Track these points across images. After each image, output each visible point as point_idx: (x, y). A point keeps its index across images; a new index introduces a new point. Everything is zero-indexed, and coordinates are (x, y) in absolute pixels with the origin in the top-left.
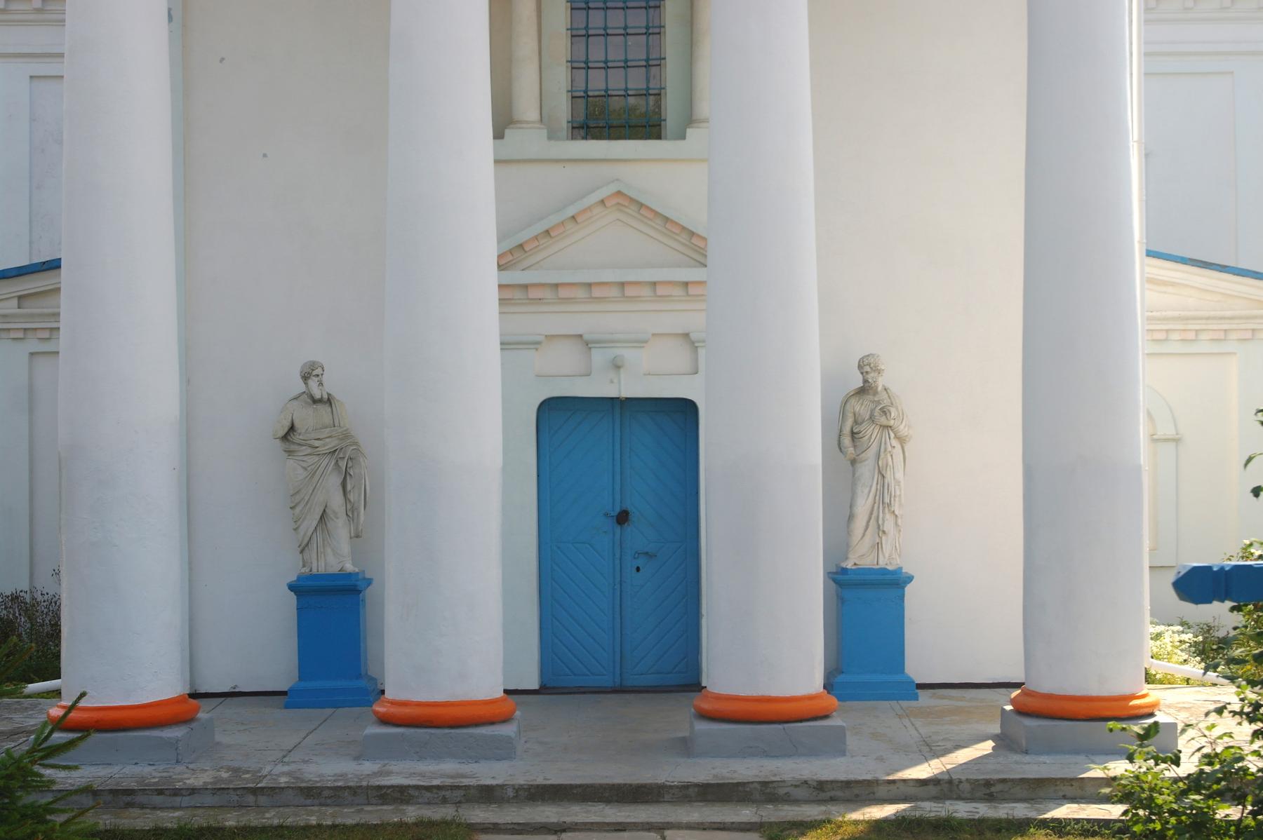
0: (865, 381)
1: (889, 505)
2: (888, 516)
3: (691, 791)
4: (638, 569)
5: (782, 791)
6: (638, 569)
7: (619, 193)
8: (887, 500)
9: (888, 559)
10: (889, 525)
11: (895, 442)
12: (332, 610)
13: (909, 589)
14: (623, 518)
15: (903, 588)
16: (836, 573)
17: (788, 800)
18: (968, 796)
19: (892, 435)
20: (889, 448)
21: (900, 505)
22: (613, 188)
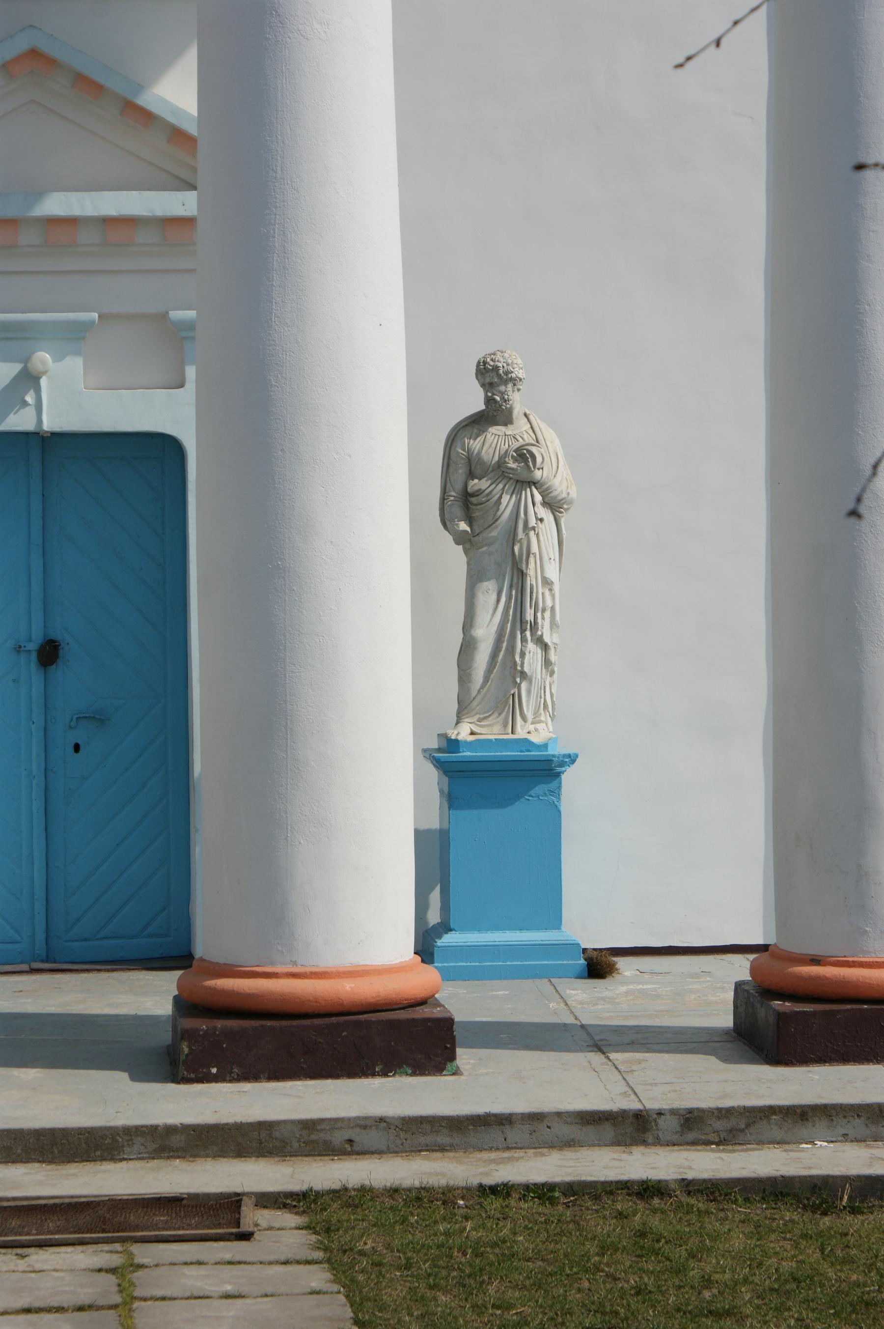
0: (489, 401)
1: (534, 626)
2: (531, 646)
3: (176, 1141)
4: (77, 748)
5: (338, 1138)
6: (77, 748)
7: (34, 54)
8: (529, 615)
9: (538, 731)
10: (532, 659)
11: (543, 512)
12: (113, 1271)
13: (569, 777)
14: (49, 654)
15: (558, 775)
16: (439, 750)
17: (349, 1149)
18: (675, 1138)
19: (538, 498)
20: (532, 522)
21: (553, 624)
22: (21, 44)
